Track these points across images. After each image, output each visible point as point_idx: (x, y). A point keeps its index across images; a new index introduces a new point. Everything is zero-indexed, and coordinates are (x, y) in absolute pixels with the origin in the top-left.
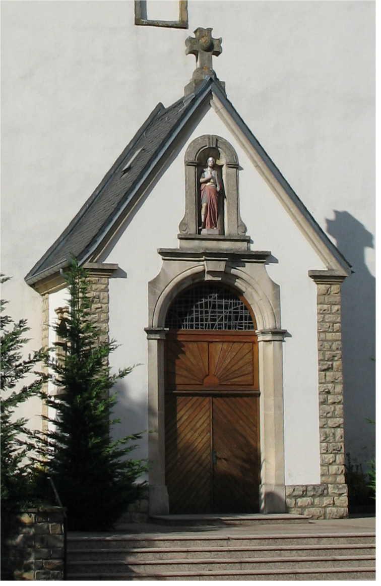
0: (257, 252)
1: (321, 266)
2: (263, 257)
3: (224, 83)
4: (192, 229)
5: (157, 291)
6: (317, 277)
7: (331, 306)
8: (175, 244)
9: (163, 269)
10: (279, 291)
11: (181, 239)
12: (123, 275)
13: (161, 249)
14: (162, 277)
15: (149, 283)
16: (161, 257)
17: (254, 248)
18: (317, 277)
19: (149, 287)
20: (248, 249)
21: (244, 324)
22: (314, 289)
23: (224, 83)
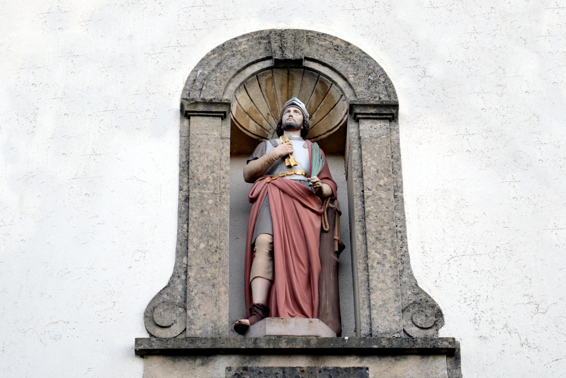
4: (213, 315)
11: (143, 352)
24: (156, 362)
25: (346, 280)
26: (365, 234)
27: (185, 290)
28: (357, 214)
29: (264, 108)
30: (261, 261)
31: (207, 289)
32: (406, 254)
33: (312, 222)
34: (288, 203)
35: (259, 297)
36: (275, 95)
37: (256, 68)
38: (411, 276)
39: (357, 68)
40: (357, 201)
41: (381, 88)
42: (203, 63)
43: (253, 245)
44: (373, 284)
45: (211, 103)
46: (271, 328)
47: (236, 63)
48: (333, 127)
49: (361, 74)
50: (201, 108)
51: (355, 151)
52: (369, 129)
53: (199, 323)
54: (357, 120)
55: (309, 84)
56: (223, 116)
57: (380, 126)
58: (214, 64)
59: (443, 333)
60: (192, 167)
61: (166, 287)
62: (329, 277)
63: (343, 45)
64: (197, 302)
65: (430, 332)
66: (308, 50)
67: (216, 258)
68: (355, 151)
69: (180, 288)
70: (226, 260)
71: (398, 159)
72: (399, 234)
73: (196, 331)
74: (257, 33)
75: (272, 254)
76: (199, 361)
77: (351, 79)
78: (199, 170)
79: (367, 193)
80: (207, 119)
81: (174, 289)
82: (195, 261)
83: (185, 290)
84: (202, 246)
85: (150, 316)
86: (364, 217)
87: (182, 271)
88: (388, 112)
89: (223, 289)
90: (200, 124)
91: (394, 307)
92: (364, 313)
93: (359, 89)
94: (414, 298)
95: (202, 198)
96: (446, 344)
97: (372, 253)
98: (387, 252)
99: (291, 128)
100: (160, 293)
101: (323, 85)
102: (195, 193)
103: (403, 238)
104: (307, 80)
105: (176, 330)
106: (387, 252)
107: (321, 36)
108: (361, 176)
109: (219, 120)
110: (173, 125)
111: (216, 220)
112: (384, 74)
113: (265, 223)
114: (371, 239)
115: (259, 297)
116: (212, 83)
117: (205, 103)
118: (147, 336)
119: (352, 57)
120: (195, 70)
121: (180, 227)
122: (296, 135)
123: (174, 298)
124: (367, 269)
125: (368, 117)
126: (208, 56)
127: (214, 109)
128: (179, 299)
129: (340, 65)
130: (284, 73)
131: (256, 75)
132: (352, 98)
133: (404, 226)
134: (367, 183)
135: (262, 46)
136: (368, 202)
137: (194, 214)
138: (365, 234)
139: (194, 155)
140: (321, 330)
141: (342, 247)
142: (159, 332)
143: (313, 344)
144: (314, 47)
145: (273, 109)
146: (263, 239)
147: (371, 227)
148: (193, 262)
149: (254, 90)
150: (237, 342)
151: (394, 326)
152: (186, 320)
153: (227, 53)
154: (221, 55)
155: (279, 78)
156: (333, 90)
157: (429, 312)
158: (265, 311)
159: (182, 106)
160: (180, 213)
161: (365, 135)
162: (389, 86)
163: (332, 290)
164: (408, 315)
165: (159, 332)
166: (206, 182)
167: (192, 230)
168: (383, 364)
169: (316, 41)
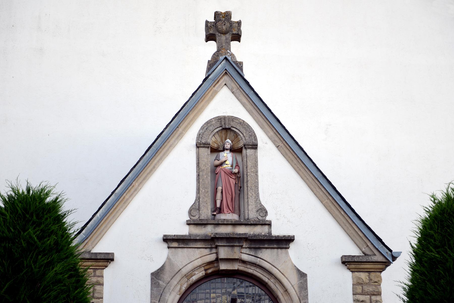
0: (278, 236)
1: (353, 251)
2: (284, 242)
3: (241, 63)
4: (206, 212)
5: (161, 282)
6: (348, 262)
7: (370, 297)
8: (184, 231)
9: (168, 258)
10: (306, 281)
11: (188, 224)
12: (167, 240)
13: (165, 236)
14: (167, 268)
15: (152, 274)
16: (165, 245)
17: (277, 231)
18: (348, 262)
19: (152, 279)
20: (270, 233)
21: (245, 295)
22: (346, 277)
23: (241, 63)
24: (192, 226)
25: (242, 196)
26: (247, 187)
27: (199, 204)
28: (245, 173)
29: (219, 140)
30: (219, 195)
31: (205, 204)
32: (258, 194)
33: (233, 181)
34: (226, 176)
35: (218, 205)
36: (222, 136)
37: (217, 130)
38: (260, 200)
39: (246, 130)
40: (245, 176)
41: (253, 138)
42: (202, 128)
43: (217, 189)
44: (249, 203)
45: (205, 144)
46: (222, 217)
47: (211, 128)
48: (251, 256)
49: (247, 133)
50: (202, 145)
51: (245, 159)
52: (249, 152)
53: (203, 215)
54: (246, 148)
55: (232, 134)
56: (208, 147)
57: (252, 151)
58: (205, 128)
59: (268, 218)
60: (200, 165)
61: (198, 175)
62: (237, 198)
63: (242, 122)
64: (202, 208)
65: (264, 218)
66: (232, 124)
67: (207, 195)
68: (245, 159)
69: (198, 204)
70: (210, 195)
71: (257, 162)
72: (257, 187)
73: (202, 217)
74: (217, 117)
75: (222, 192)
76: (203, 226)
77: (245, 135)
78: (201, 166)
79: (248, 174)
80: (204, 148)
81: (196, 204)
82: (201, 196)
83: (199, 204)
84: (203, 191)
85: (190, 212)
86: (247, 181)
87: (198, 198)
88: (255, 147)
89: (209, 204)
90: (202, 150)
91: (255, 210)
92: (247, 212)
93: (247, 138)
94: (260, 207)
95: (203, 175)
96: (268, 223)
97: (249, 193)
98: (253, 193)
99: (227, 149)
100: (192, 206)
101: (236, 135)
102: (201, 173)
103: (258, 188)
104: (232, 132)
105: (197, 217)
106: (253, 193)
107: (236, 118)
108: (247, 168)
109: (207, 149)
110: (194, 151)
111: (207, 183)
112: (254, 132)
113: (220, 183)
114: (249, 189)
115: (218, 205)
116: (205, 136)
117: (203, 144)
118: (189, 219)
119: (245, 126)
120: (200, 131)
121: (197, 184)
122: (228, 152)
123: (195, 208)
124: (248, 198)
125: (249, 148)
126: (203, 125)
127: (206, 146)
128: (197, 207)
129: (242, 129)
130: (225, 131)
131: (217, 132)
132: (245, 141)
133: (258, 184)
134: (249, 171)
135: (219, 122)
136: (249, 177)
137: (201, 181)
138: (247, 187)
139: (200, 161)
140: (234, 217)
141: (241, 187)
142: (192, 218)
143: (233, 223)
144: (234, 123)
145: (222, 140)
146: (220, 188)
147: (249, 185)
148: (201, 196)
149: (217, 136)
150: (213, 222)
151: (254, 216)
152: (200, 215)
153: (209, 125)
154: (207, 125)
155: (224, 132)
156: (239, 136)
157: (264, 212)
158: (220, 210)
159: (196, 145)
160: (197, 180)
161: (248, 154)
162: (256, 139)
163: (238, 202)
164: (258, 213)
165: (192, 218)
166: (204, 170)
167: (200, 186)
168: (252, 233)
169: (234, 120)
